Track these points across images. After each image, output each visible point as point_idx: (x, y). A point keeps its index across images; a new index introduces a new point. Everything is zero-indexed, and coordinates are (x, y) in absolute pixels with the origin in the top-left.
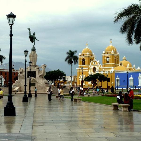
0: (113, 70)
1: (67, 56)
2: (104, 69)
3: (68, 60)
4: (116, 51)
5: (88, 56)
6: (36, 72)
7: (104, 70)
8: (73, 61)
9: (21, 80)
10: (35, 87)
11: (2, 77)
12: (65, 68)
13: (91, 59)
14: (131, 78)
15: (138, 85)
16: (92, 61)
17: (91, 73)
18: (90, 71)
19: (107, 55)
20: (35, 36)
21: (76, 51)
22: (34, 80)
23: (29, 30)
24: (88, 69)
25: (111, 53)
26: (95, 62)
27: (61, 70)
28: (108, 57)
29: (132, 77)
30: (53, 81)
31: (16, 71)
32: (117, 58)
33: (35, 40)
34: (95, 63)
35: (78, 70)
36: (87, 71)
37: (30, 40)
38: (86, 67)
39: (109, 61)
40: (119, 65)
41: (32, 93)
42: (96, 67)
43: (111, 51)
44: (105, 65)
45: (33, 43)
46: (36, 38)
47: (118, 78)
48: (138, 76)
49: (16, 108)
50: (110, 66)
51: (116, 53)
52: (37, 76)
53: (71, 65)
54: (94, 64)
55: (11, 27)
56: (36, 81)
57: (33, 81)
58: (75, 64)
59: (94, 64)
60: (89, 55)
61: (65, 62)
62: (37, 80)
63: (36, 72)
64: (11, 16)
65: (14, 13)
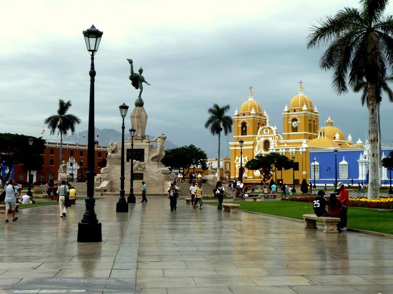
0: (305, 145)
1: (209, 116)
2: (287, 144)
3: (211, 125)
4: (311, 106)
5: (254, 116)
6: (144, 150)
7: (286, 145)
8: (222, 127)
9: (114, 167)
10: (142, 181)
11: (74, 161)
12: (205, 141)
13: (259, 124)
14: (344, 162)
15: (359, 176)
16: (262, 127)
18: (256, 148)
19: (293, 115)
20: (142, 74)
21: (228, 107)
22: (140, 166)
23: (131, 62)
24: (254, 145)
25: (302, 111)
26: (268, 130)
27: (197, 146)
28: (294, 120)
29: (346, 160)
32: (314, 122)
34: (268, 132)
35: (232, 146)
36: (252, 147)
37: (132, 84)
38: (248, 139)
39: (297, 128)
40: (319, 136)
42: (270, 139)
43: (302, 105)
44: (288, 135)
45: (139, 90)
46: (145, 80)
47: (317, 163)
48: (358, 158)
50: (299, 137)
51: (312, 111)
52: (146, 158)
53: (218, 135)
54: (265, 133)
55: (92, 55)
56: (144, 168)
58: (226, 132)
59: (265, 133)
60: (254, 114)
61: (205, 128)
62: (146, 167)
63: (144, 150)
64: (93, 34)
65: (99, 28)
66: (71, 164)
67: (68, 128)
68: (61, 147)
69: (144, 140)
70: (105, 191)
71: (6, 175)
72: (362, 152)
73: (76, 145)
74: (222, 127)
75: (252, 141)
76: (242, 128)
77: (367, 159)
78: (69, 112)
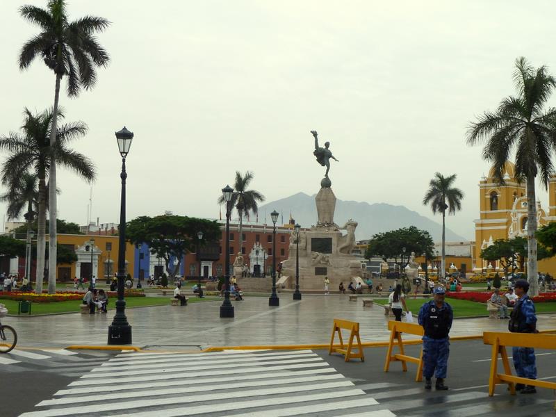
1: (427, 188)
3: (431, 202)
6: (331, 239)
8: (447, 202)
11: (261, 248)
12: (428, 219)
13: (515, 194)
17: (516, 233)
18: (511, 228)
21: (453, 177)
22: (323, 259)
23: (315, 134)
24: (508, 223)
30: (396, 258)
33: (331, 159)
36: (505, 227)
41: (302, 292)
44: (486, 214)
45: (326, 167)
52: (334, 248)
53: (442, 215)
54: (523, 206)
56: (328, 261)
58: (450, 211)
59: (523, 206)
61: (424, 207)
62: (330, 260)
63: (331, 239)
64: (125, 135)
65: (130, 130)
66: (257, 252)
67: (249, 208)
69: (330, 228)
70: (283, 287)
71: (175, 268)
73: (263, 227)
74: (447, 202)
76: (492, 200)
78: (248, 188)
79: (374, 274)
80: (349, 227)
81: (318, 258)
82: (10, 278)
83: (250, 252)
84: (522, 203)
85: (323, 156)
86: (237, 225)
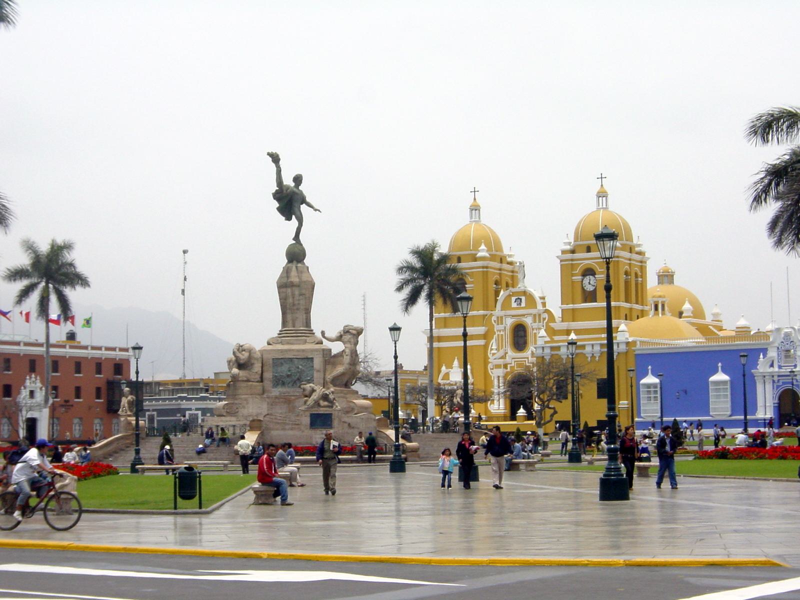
2: (577, 332)
11: (39, 384)
15: (756, 409)
16: (508, 292)
18: (493, 344)
20: (300, 188)
23: (275, 158)
24: (486, 336)
28: (589, 272)
29: (724, 371)
31: (26, 344)
32: (636, 274)
34: (523, 305)
36: (482, 342)
37: (279, 209)
42: (528, 321)
44: (573, 310)
45: (294, 222)
46: (308, 200)
48: (755, 364)
49: (598, 498)
54: (514, 305)
57: (319, 405)
59: (514, 305)
60: (483, 258)
68: (48, 352)
72: (765, 351)
75: (483, 326)
77: (776, 369)
79: (491, 432)
80: (347, 337)
81: (315, 396)
82: (526, 452)
83: (19, 393)
84: (513, 299)
85: (289, 202)
86: (41, 345)
